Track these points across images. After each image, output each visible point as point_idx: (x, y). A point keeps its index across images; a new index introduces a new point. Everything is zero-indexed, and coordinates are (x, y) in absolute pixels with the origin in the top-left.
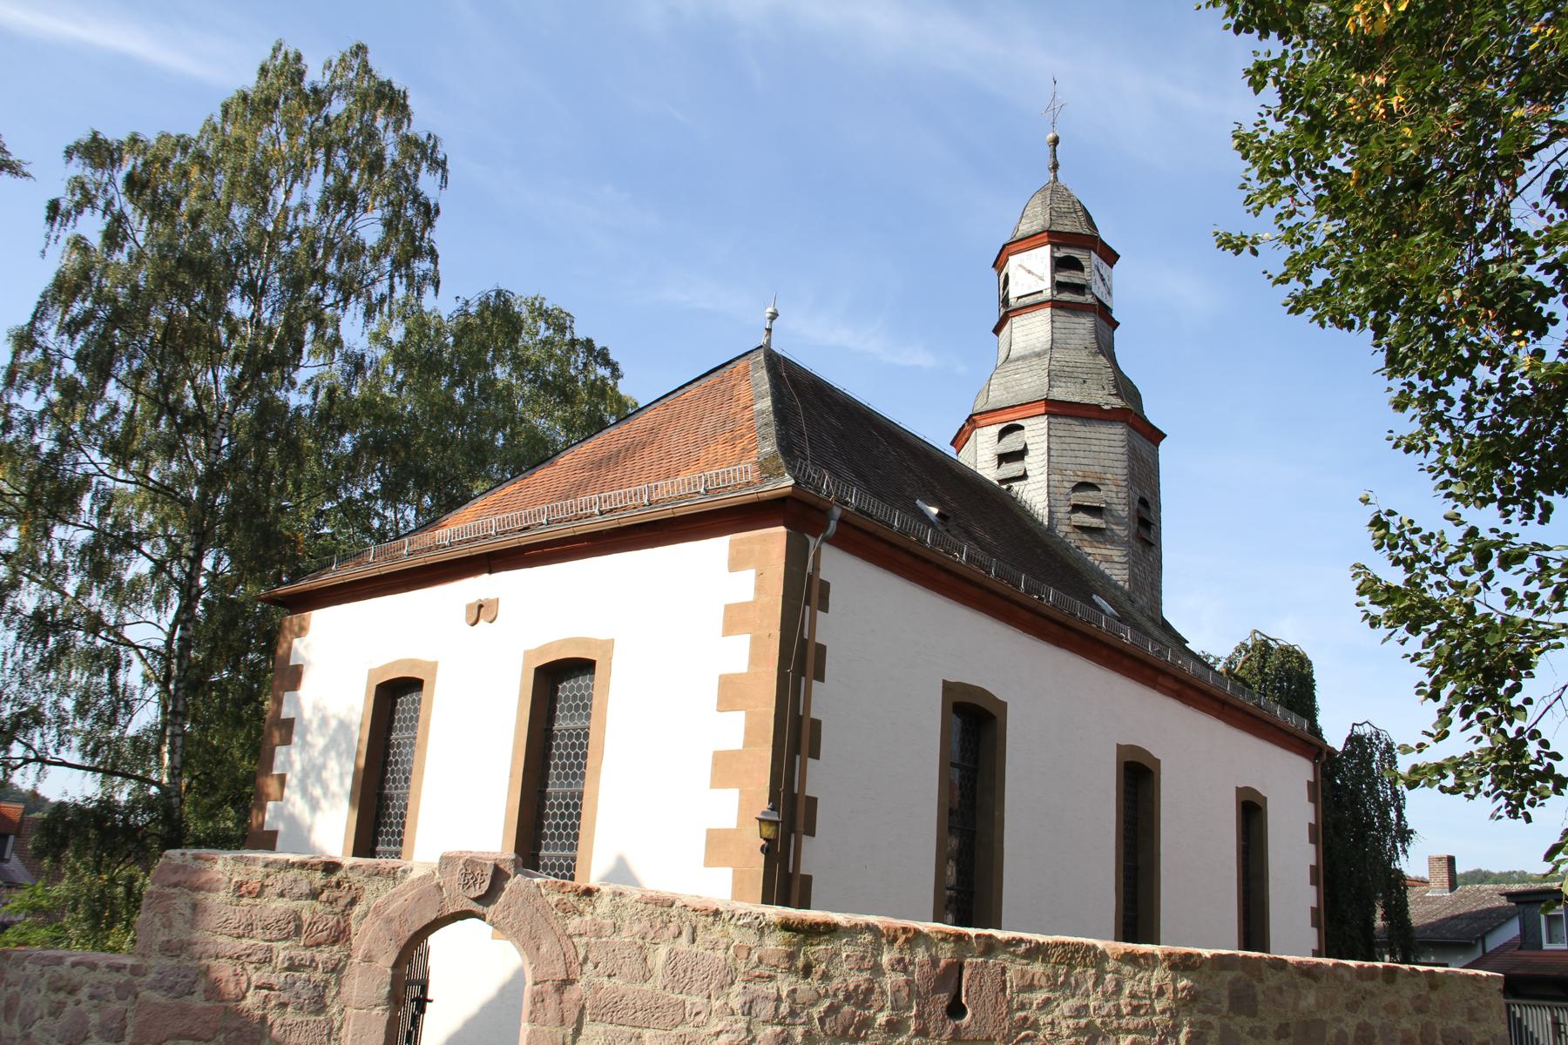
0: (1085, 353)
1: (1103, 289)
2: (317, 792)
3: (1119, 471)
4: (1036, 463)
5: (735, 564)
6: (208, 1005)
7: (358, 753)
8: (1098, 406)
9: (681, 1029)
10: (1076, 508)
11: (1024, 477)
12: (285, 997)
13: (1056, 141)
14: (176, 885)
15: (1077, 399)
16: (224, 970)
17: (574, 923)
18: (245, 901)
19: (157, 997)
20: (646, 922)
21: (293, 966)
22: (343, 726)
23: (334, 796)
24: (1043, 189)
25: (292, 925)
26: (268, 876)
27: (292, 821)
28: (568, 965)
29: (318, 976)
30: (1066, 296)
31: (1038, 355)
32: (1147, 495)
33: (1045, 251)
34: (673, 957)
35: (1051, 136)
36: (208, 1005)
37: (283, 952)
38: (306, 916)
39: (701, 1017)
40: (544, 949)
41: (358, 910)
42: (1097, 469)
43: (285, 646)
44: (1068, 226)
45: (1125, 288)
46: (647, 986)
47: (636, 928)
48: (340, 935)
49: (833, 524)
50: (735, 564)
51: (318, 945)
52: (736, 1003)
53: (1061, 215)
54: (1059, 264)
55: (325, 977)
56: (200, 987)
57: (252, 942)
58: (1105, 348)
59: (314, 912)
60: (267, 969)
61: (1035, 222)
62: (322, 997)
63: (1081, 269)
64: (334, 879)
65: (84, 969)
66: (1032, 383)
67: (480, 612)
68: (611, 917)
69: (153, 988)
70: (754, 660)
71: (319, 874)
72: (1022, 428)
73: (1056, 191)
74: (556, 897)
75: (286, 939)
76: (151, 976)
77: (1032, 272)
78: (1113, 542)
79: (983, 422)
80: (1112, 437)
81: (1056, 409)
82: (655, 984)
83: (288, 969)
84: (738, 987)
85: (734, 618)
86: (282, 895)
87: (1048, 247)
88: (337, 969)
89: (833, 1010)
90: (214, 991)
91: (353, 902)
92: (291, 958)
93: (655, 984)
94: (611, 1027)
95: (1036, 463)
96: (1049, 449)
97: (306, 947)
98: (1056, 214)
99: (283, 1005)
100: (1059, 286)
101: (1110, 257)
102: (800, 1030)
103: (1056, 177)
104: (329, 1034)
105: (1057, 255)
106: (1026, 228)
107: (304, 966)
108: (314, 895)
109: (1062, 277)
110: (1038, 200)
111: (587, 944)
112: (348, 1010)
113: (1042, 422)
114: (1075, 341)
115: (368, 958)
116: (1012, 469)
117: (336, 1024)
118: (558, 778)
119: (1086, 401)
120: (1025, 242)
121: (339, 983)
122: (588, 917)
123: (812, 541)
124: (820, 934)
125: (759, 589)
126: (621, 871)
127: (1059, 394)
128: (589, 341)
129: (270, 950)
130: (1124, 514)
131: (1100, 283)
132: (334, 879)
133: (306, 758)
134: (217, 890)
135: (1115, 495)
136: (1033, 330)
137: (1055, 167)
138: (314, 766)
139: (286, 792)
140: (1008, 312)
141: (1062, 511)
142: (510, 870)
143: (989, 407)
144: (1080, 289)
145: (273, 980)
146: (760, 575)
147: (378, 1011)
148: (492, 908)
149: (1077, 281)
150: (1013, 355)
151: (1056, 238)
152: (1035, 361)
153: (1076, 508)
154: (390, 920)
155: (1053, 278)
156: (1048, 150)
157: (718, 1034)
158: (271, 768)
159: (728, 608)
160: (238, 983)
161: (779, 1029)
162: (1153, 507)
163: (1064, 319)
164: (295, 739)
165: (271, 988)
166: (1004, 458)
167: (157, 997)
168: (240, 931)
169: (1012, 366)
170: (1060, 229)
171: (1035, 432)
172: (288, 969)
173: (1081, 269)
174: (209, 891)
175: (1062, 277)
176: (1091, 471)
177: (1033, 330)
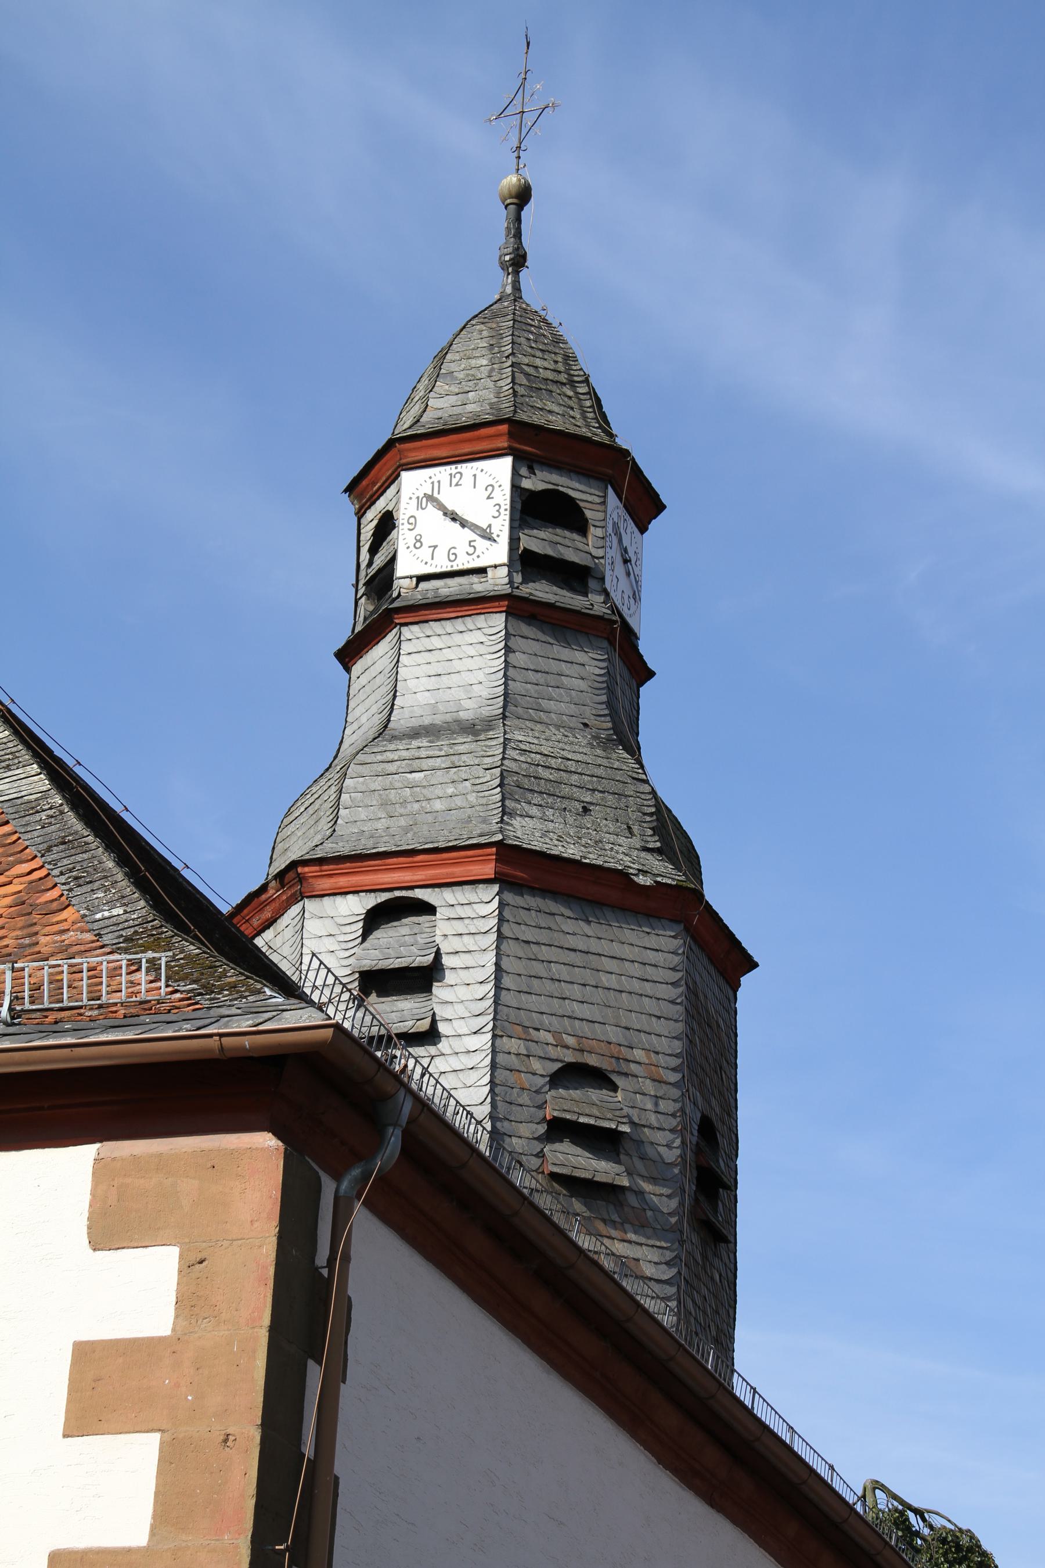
0: (583, 739)
1: (624, 584)
3: (662, 1044)
4: (462, 1002)
5: (112, 1226)
8: (622, 877)
10: (559, 1129)
11: (430, 1036)
13: (522, 196)
15: (572, 852)
24: (486, 315)
30: (543, 591)
31: (472, 729)
32: (715, 1112)
35: (512, 180)
42: (613, 1034)
44: (554, 414)
45: (669, 583)
49: (394, 1140)
50: (112, 1226)
53: (538, 385)
54: (529, 509)
58: (623, 732)
61: (473, 389)
63: (580, 526)
66: (455, 799)
70: (169, 1509)
72: (429, 909)
73: (522, 330)
77: (458, 517)
78: (642, 1226)
79: (326, 884)
80: (649, 957)
81: (523, 873)
85: (104, 1387)
95: (462, 1002)
96: (499, 970)
98: (526, 381)
100: (525, 562)
101: (645, 505)
103: (517, 287)
105: (526, 484)
106: (445, 405)
109: (540, 540)
110: (478, 338)
114: (559, 707)
116: (400, 1012)
119: (593, 858)
123: (329, 1187)
125: (190, 1302)
127: (530, 831)
130: (671, 1155)
131: (620, 569)
135: (647, 1104)
136: (454, 667)
137: (518, 261)
140: (386, 608)
141: (523, 1137)
143: (344, 848)
144: (577, 576)
146: (192, 1265)
149: (571, 556)
150: (400, 720)
151: (528, 443)
152: (464, 744)
153: (559, 1129)
155: (514, 541)
156: (501, 217)
159: (85, 1354)
162: (723, 1142)
163: (538, 648)
166: (377, 982)
169: (401, 750)
170: (537, 419)
171: (465, 926)
173: (580, 526)
175: (540, 540)
176: (599, 1036)
177: (454, 667)
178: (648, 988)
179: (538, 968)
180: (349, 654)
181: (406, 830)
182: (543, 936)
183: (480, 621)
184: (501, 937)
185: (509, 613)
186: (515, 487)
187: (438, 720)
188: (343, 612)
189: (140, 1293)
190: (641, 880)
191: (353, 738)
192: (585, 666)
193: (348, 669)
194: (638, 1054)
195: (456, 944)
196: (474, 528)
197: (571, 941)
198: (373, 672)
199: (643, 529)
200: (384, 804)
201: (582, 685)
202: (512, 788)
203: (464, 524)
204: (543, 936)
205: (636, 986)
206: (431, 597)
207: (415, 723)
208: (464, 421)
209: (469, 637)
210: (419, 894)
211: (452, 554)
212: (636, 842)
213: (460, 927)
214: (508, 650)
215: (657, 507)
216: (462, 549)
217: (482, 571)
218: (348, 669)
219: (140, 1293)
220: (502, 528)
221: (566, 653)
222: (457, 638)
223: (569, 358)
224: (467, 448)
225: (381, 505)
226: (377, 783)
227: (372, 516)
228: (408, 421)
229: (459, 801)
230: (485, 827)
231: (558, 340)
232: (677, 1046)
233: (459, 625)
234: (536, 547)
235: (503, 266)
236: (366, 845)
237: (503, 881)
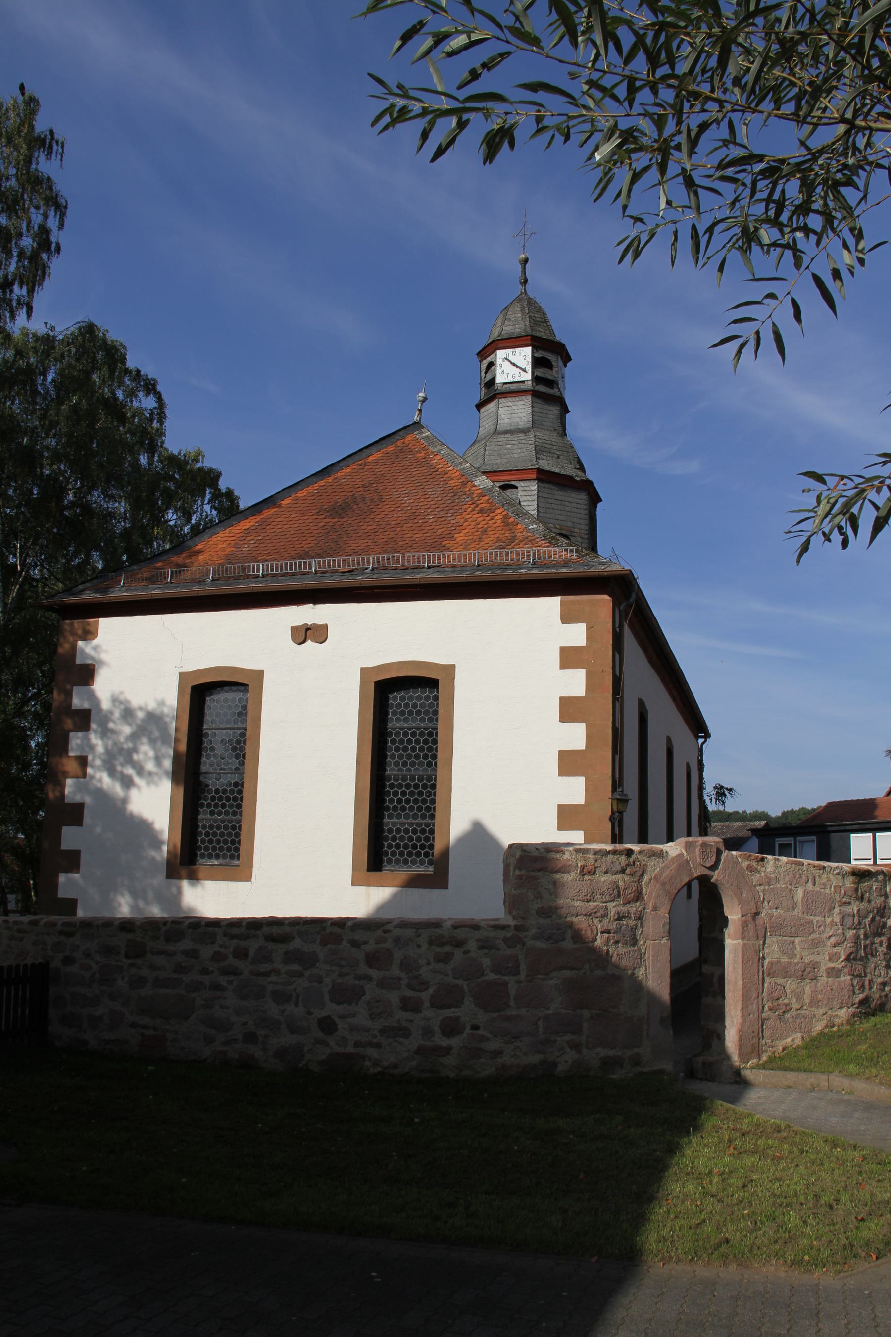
0: (555, 434)
2: (130, 771)
3: (583, 527)
5: (567, 618)
6: (575, 946)
7: (177, 740)
8: (571, 478)
9: (813, 936)
12: (617, 937)
13: (526, 261)
14: (539, 870)
15: (557, 470)
16: (581, 922)
17: (756, 878)
18: (586, 877)
19: (540, 944)
20: (791, 875)
21: (620, 917)
22: (153, 718)
23: (150, 774)
24: (518, 299)
25: (616, 892)
26: (596, 860)
27: (102, 795)
28: (756, 903)
29: (632, 922)
30: (542, 388)
31: (525, 431)
33: (528, 350)
34: (806, 893)
36: (575, 946)
37: (613, 908)
38: (621, 884)
39: (822, 928)
40: (744, 895)
41: (646, 878)
42: (569, 524)
43: (67, 646)
44: (542, 333)
45: (573, 382)
46: (795, 913)
47: (787, 879)
48: (638, 896)
50: (567, 618)
51: (629, 903)
52: (837, 919)
54: (537, 362)
55: (635, 922)
56: (569, 934)
57: (596, 904)
59: (625, 883)
60: (606, 920)
61: (517, 324)
62: (635, 935)
64: (631, 860)
65: (467, 929)
67: (306, 634)
68: (774, 873)
69: (535, 938)
71: (623, 858)
72: (516, 488)
74: (747, 863)
75: (613, 900)
76: (533, 931)
77: (514, 365)
81: (544, 477)
82: (798, 912)
83: (617, 919)
84: (837, 910)
85: (569, 658)
86: (606, 872)
87: (530, 348)
88: (640, 917)
89: (873, 919)
90: (577, 936)
91: (642, 875)
92: (618, 913)
93: (798, 912)
94: (780, 938)
97: (624, 904)
99: (617, 942)
100: (536, 379)
101: (567, 359)
102: (862, 931)
104: (641, 958)
105: (536, 355)
106: (509, 329)
107: (624, 917)
108: (623, 871)
109: (540, 372)
110: (517, 308)
111: (764, 890)
112: (648, 942)
113: (534, 487)
115: (655, 909)
117: (643, 951)
118: (397, 764)
120: (513, 342)
121: (642, 926)
122: (763, 874)
124: (866, 876)
126: (478, 831)
127: (546, 464)
128: (138, 371)
129: (606, 908)
132: (631, 860)
133: (110, 743)
134: (569, 872)
137: (525, 282)
138: (121, 750)
139: (89, 771)
142: (723, 849)
144: (551, 383)
145: (610, 927)
147: (664, 941)
148: (717, 872)
151: (537, 343)
152: (522, 436)
154: (663, 884)
156: (519, 268)
157: (830, 937)
158: (67, 751)
160: (592, 931)
161: (854, 932)
164: (93, 726)
165: (608, 932)
167: (540, 944)
168: (588, 897)
169: (502, 438)
170: (538, 334)
172: (617, 919)
174: (564, 872)
175: (540, 372)
177: (517, 412)
178: (578, 511)
179: (549, 505)
180: (479, 406)
181: (507, 463)
182: (549, 496)
183: (524, 397)
184: (538, 496)
185: (532, 395)
186: (533, 356)
187: (512, 428)
188: (479, 393)
189: (577, 635)
190: (577, 479)
191: (482, 432)
192: (555, 410)
193: (479, 411)
194: (576, 530)
195: (525, 498)
196: (520, 368)
197: (558, 497)
198: (489, 412)
199: (566, 366)
200: (499, 454)
201: (552, 417)
202: (539, 451)
203: (517, 367)
204: (549, 496)
205: (575, 510)
206: (508, 390)
207: (505, 429)
208: (516, 335)
209: (520, 403)
210: (513, 483)
211: (514, 377)
212: (573, 466)
213: (525, 493)
214: (532, 407)
215: (570, 359)
216: (517, 375)
217: (523, 382)
218: (479, 411)
219: (577, 635)
220: (529, 368)
221: (549, 407)
222: (516, 403)
223: (544, 314)
224: (518, 343)
225: (489, 359)
226: (496, 448)
227: (485, 363)
228: (496, 334)
229: (522, 454)
230: (532, 464)
231: (540, 308)
232: (587, 528)
233: (517, 399)
234: (540, 375)
235: (521, 283)
236: (495, 468)
237: (539, 480)
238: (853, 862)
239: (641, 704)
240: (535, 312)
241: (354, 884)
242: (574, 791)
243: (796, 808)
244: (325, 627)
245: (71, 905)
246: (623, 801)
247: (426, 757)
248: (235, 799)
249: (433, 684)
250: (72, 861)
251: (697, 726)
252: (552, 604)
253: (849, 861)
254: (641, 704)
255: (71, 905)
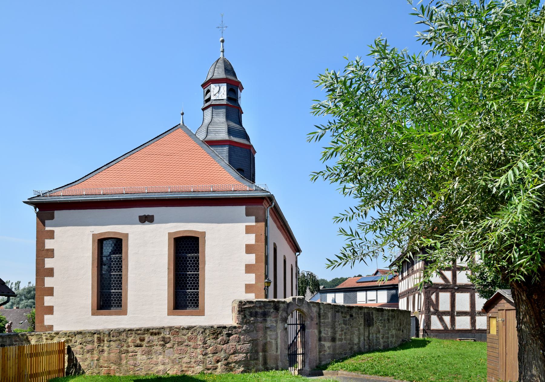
45: (245, 100)
227: (206, 89)
238: (358, 303)
239: (275, 244)
240: (229, 69)
241: (168, 315)
242: (251, 279)
243: (339, 278)
244: (153, 216)
245: (51, 327)
246: (269, 283)
247: (194, 266)
248: (118, 284)
249: (197, 239)
250: (50, 310)
251: (297, 249)
252: (242, 209)
253: (356, 303)
254: (275, 244)
255: (51, 327)
